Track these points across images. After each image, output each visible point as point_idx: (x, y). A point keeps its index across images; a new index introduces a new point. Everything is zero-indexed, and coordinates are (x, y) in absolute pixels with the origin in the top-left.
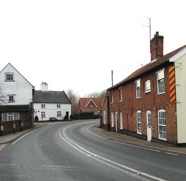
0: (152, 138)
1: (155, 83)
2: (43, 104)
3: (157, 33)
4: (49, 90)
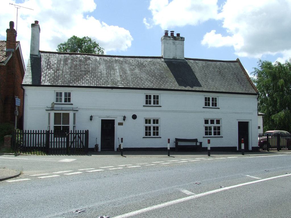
1: (110, 68)
3: (224, 19)
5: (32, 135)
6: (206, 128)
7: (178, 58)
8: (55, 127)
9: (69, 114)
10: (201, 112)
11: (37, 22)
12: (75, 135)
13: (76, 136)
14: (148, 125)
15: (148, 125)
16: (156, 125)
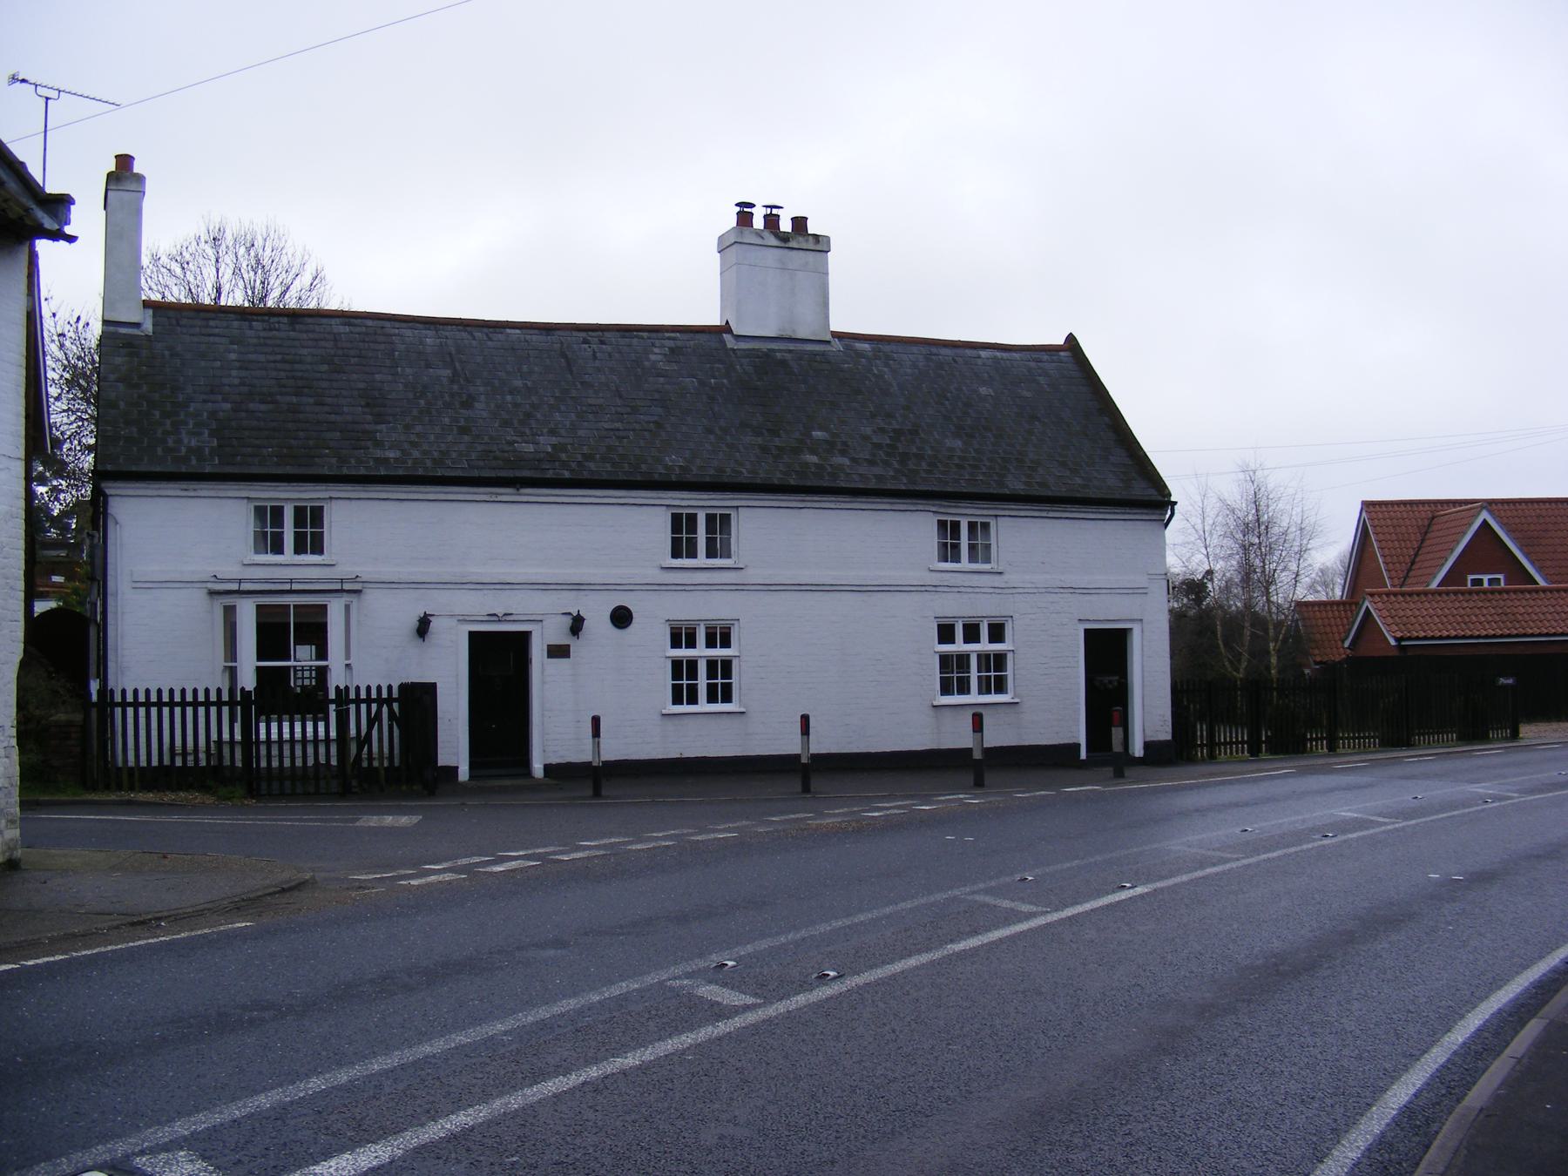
0: (105, 322)
2: (700, 505)
4: (839, 323)
5: (178, 710)
6: (945, 660)
7: (802, 333)
8: (259, 669)
9: (323, 609)
10: (923, 589)
11: (124, 161)
12: (374, 707)
13: (379, 711)
14: (683, 653)
15: (683, 653)
16: (719, 652)
